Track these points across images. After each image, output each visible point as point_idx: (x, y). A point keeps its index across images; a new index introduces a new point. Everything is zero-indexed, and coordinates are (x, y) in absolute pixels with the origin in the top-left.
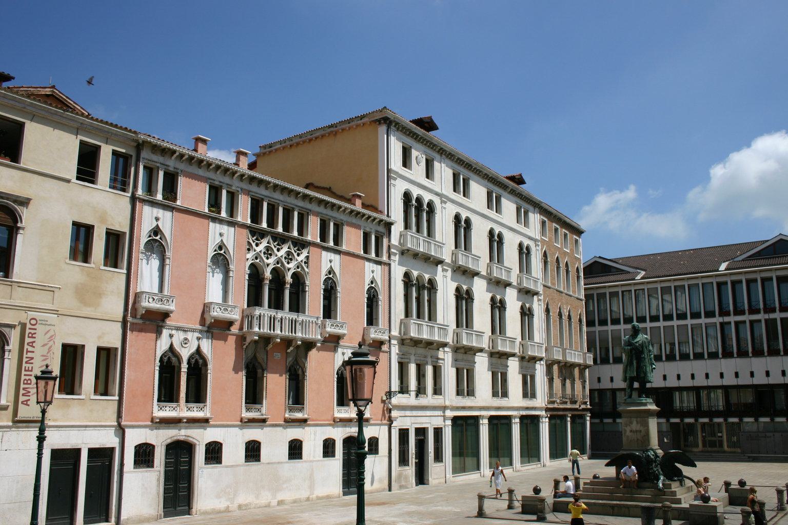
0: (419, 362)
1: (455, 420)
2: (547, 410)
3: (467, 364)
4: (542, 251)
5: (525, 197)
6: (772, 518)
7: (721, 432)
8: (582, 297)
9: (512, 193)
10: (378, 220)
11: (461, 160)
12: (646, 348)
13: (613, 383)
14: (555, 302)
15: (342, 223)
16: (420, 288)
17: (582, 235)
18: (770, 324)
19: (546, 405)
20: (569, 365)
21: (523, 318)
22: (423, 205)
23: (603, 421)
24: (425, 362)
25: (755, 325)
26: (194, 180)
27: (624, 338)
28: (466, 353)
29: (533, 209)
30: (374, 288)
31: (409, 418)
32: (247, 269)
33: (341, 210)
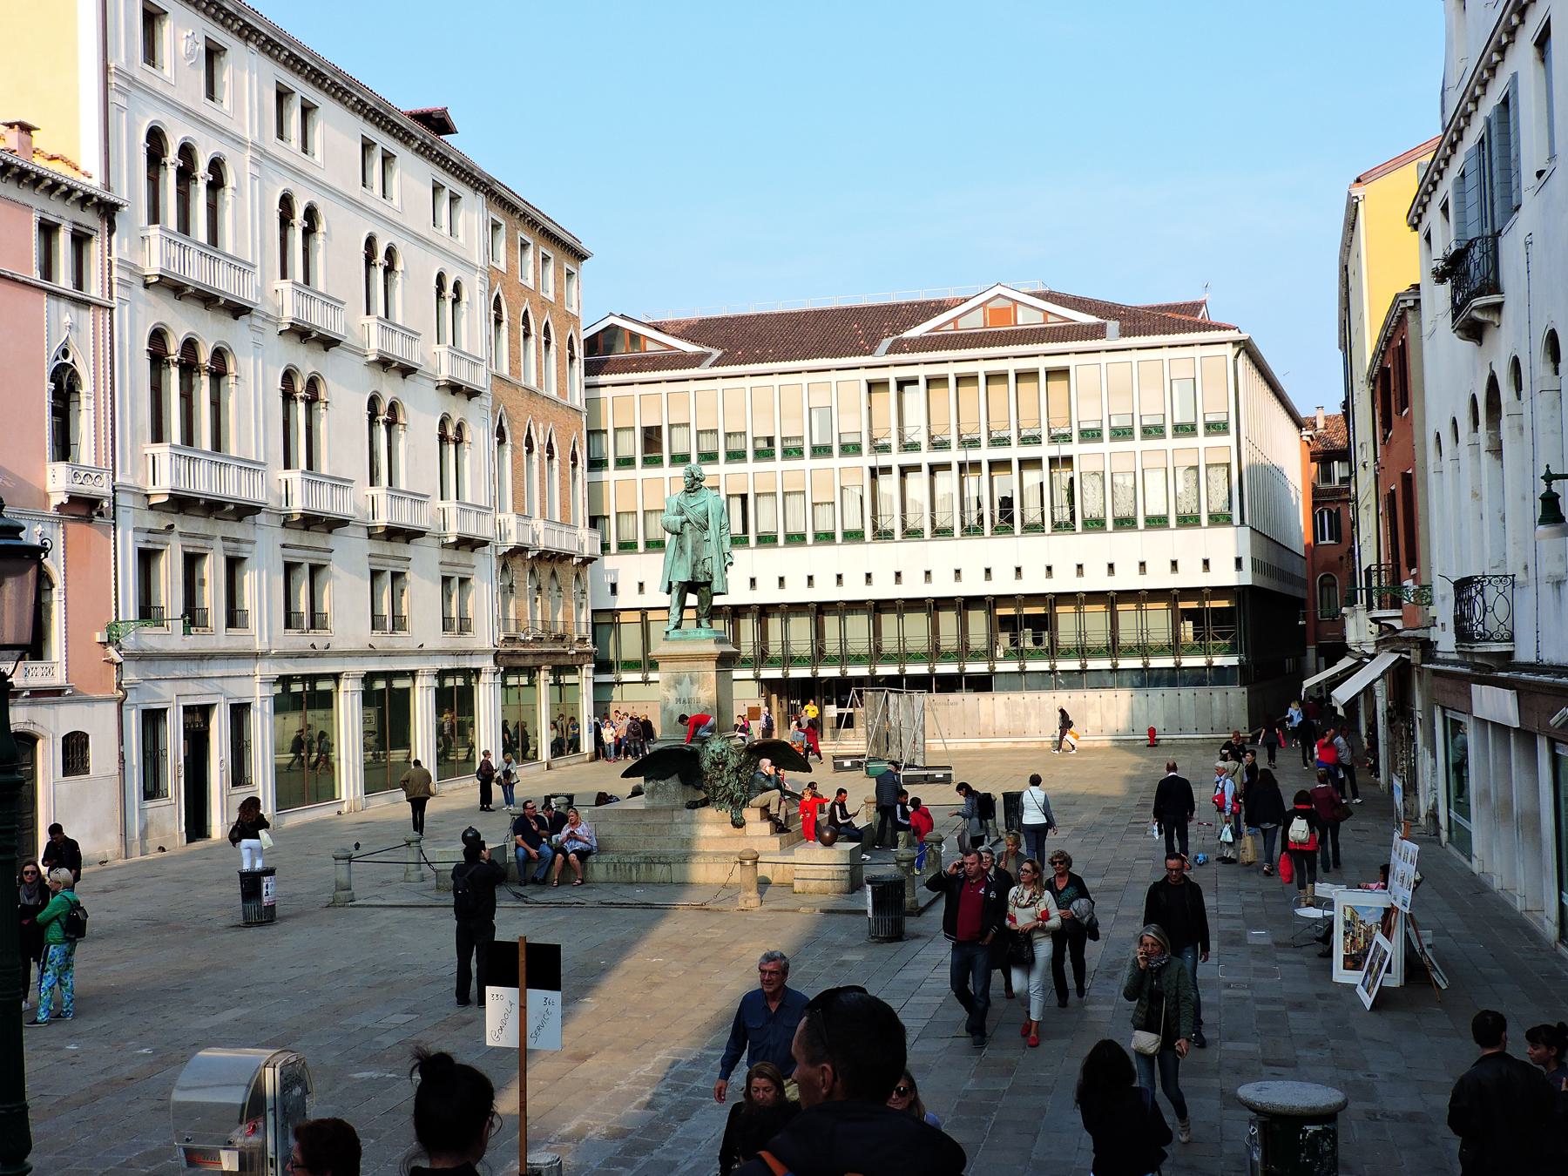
11: (298, 60)
16: (189, 368)
19: (495, 646)
21: (445, 447)
30: (70, 366)
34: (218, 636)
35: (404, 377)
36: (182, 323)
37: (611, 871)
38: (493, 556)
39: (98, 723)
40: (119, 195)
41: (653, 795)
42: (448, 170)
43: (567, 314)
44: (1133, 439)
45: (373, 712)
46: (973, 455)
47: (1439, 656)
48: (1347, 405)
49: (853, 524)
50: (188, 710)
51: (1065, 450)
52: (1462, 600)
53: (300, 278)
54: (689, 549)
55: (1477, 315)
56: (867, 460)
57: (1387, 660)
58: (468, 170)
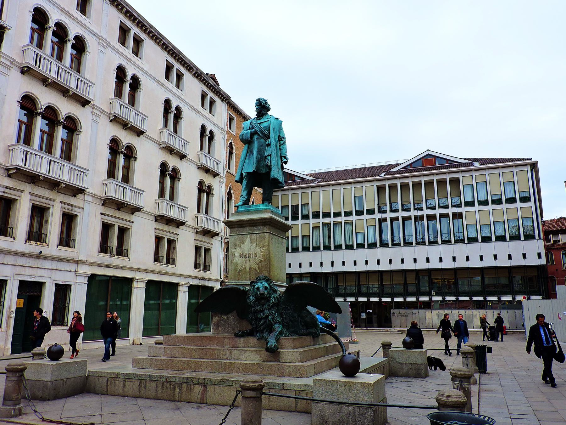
1: (92, 278)
19: (221, 279)
35: (181, 159)
37: (160, 389)
41: (218, 326)
44: (488, 205)
46: (420, 213)
49: (371, 241)
51: (459, 210)
54: (255, 152)
56: (377, 216)
58: (218, 90)
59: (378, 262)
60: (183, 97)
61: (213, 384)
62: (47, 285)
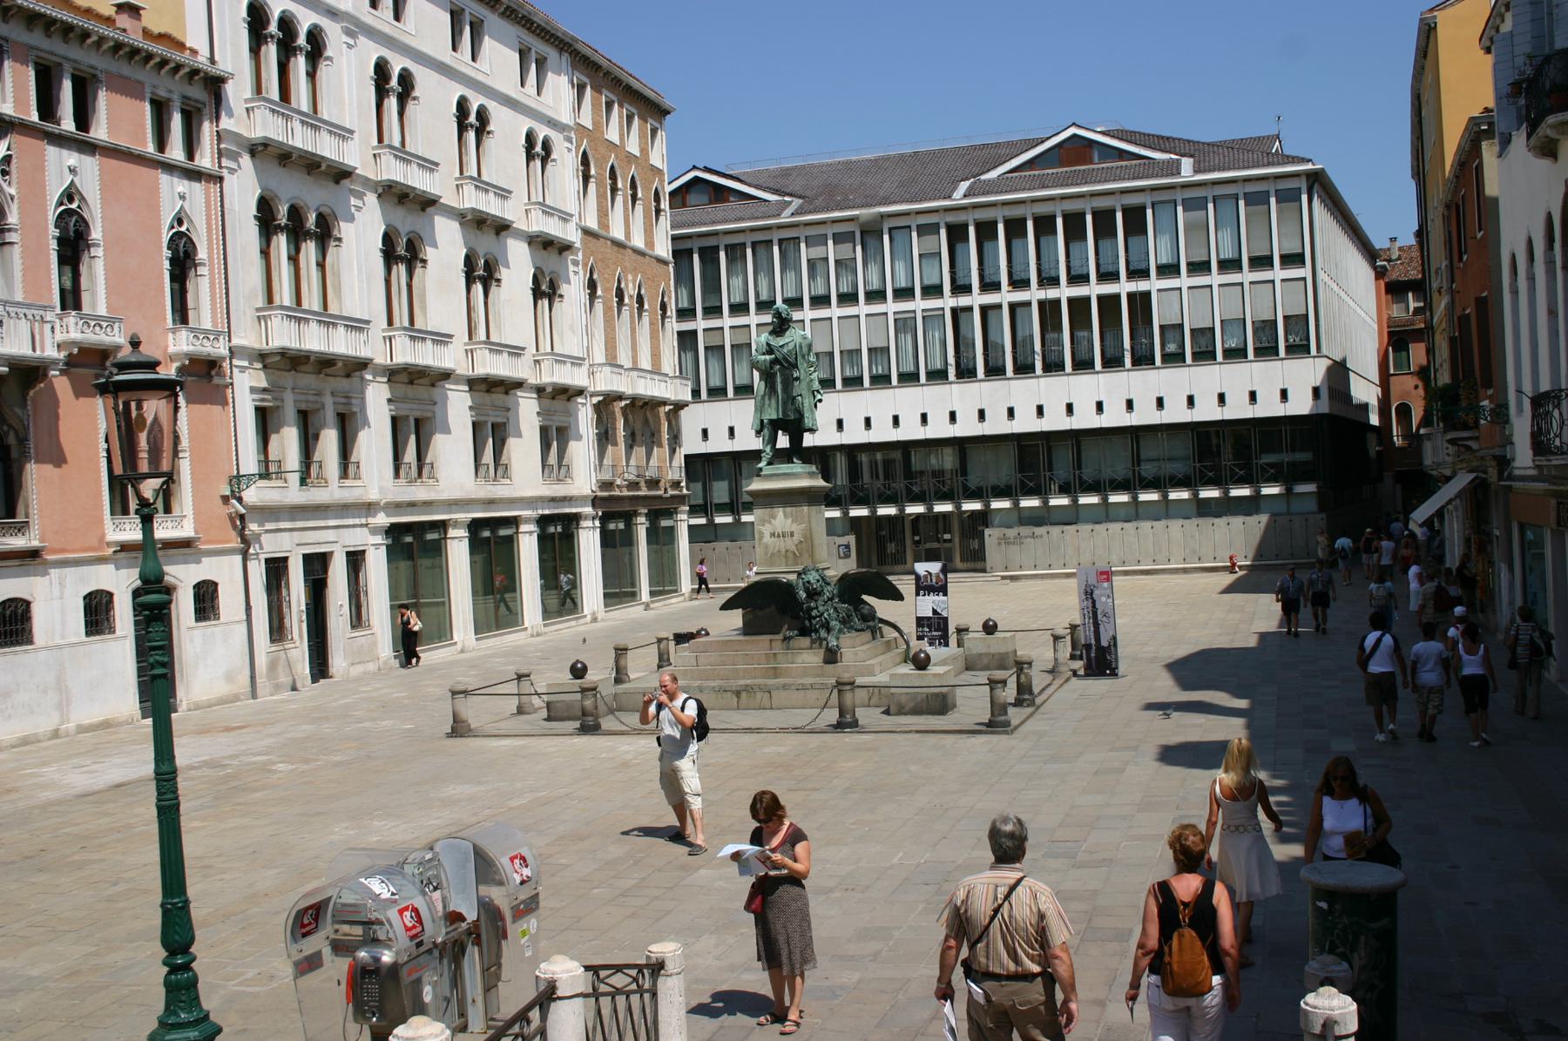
0: (303, 407)
1: (394, 531)
2: (595, 501)
3: (414, 406)
4: (577, 153)
5: (539, 26)
6: (1044, 689)
7: (949, 532)
8: (663, 249)
9: (508, 17)
10: (187, 70)
12: (803, 357)
13: (735, 440)
14: (608, 267)
15: (94, 76)
17: (668, 117)
18: (1049, 310)
19: (593, 491)
20: (641, 404)
22: (268, 22)
23: (740, 519)
24: (318, 406)
25: (1019, 311)
26: (119, 95)
27: (759, 339)
28: (411, 382)
29: (558, 55)
31: (287, 534)
32: (165, 249)
33: (89, 41)
34: (332, 491)
35: (497, 234)
36: (292, 189)
38: (588, 404)
39: (224, 571)
40: (224, 64)
42: (533, 32)
43: (653, 168)
45: (479, 558)
47: (1517, 472)
48: (1421, 234)
50: (308, 559)
52: (1539, 415)
53: (275, 95)
55: (1549, 132)
57: (1463, 480)
59: (953, 417)
60: (480, 78)
61: (778, 689)
62: (335, 555)
